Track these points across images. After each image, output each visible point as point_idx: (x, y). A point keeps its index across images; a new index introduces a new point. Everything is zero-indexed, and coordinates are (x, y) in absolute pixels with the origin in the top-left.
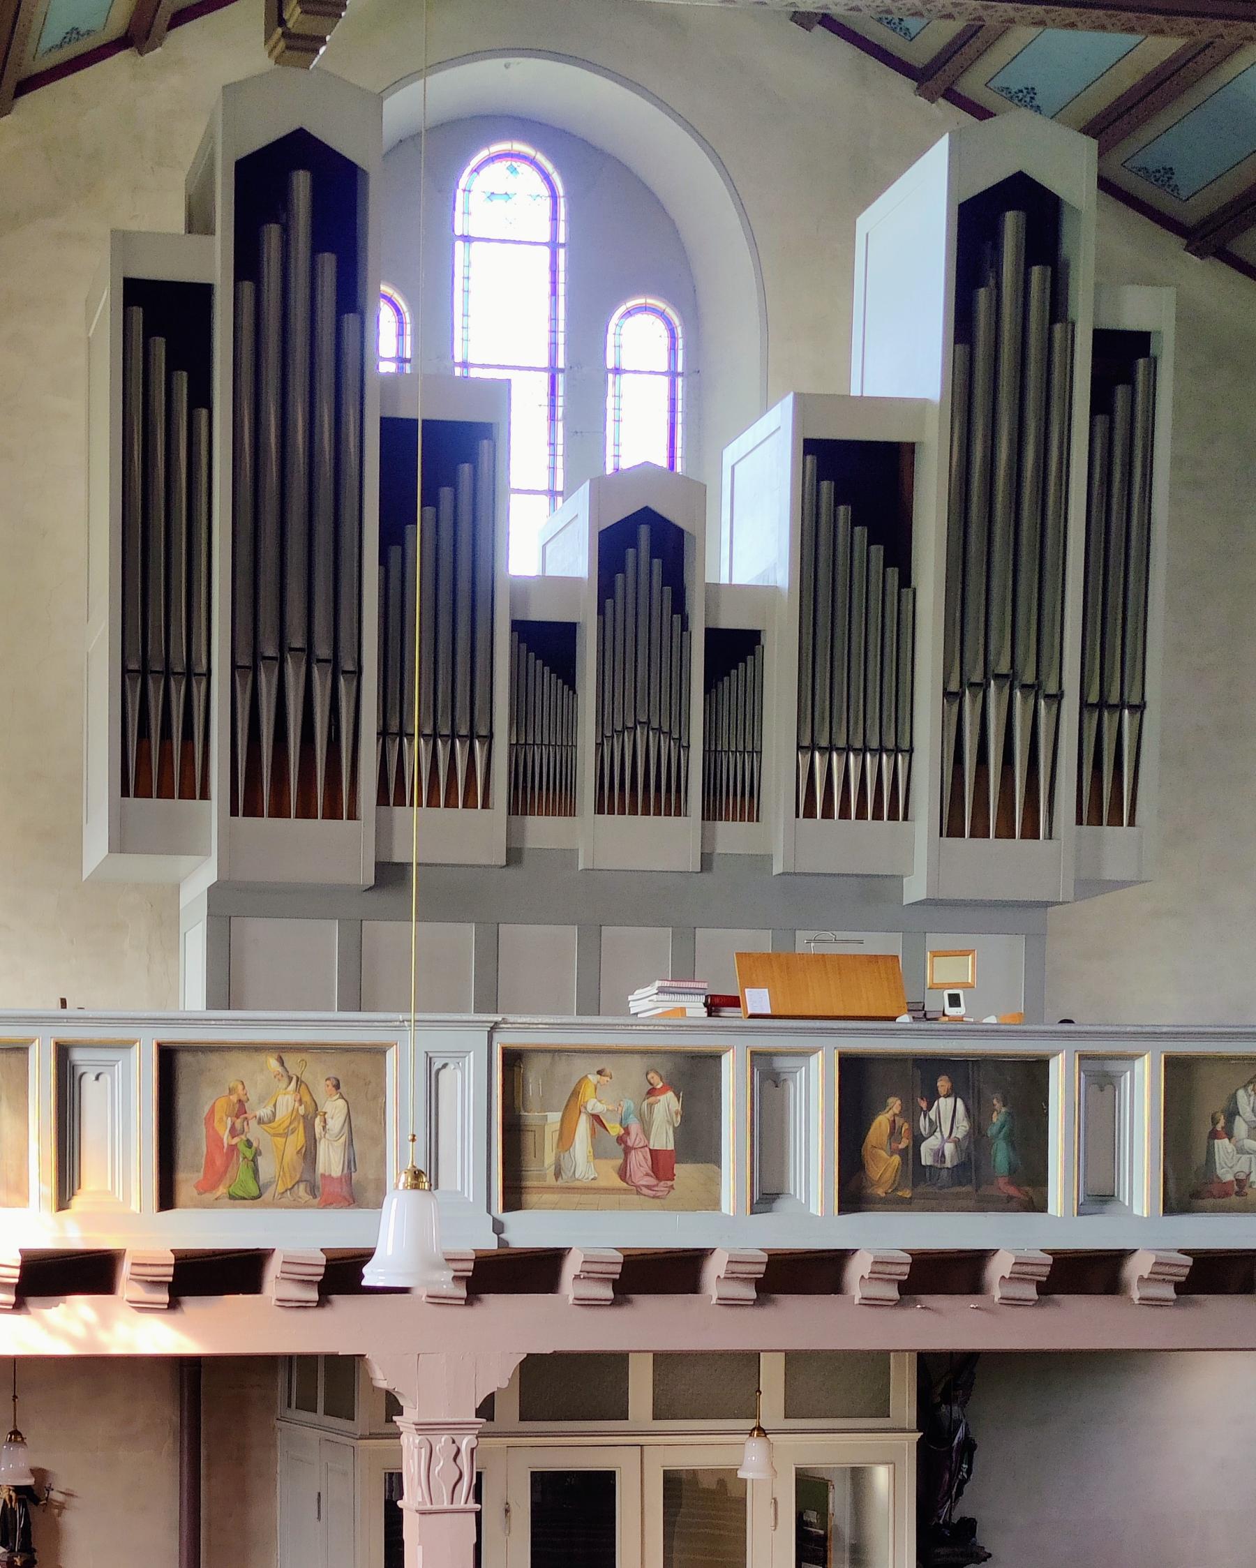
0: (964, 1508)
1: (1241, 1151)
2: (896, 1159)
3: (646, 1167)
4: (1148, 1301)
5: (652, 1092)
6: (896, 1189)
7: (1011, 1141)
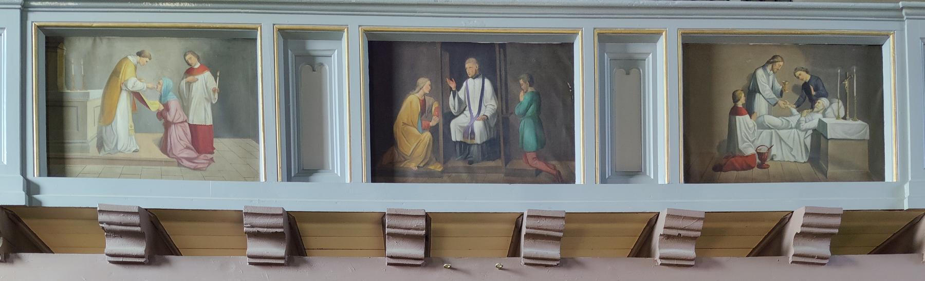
0: (163, 121)
1: (762, 126)
2: (427, 135)
3: (186, 140)
4: (671, 262)
5: (190, 71)
6: (427, 164)
7: (539, 123)
